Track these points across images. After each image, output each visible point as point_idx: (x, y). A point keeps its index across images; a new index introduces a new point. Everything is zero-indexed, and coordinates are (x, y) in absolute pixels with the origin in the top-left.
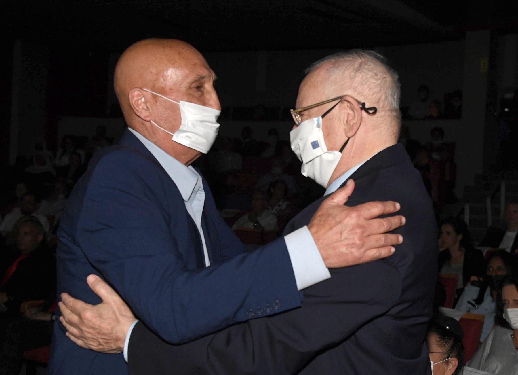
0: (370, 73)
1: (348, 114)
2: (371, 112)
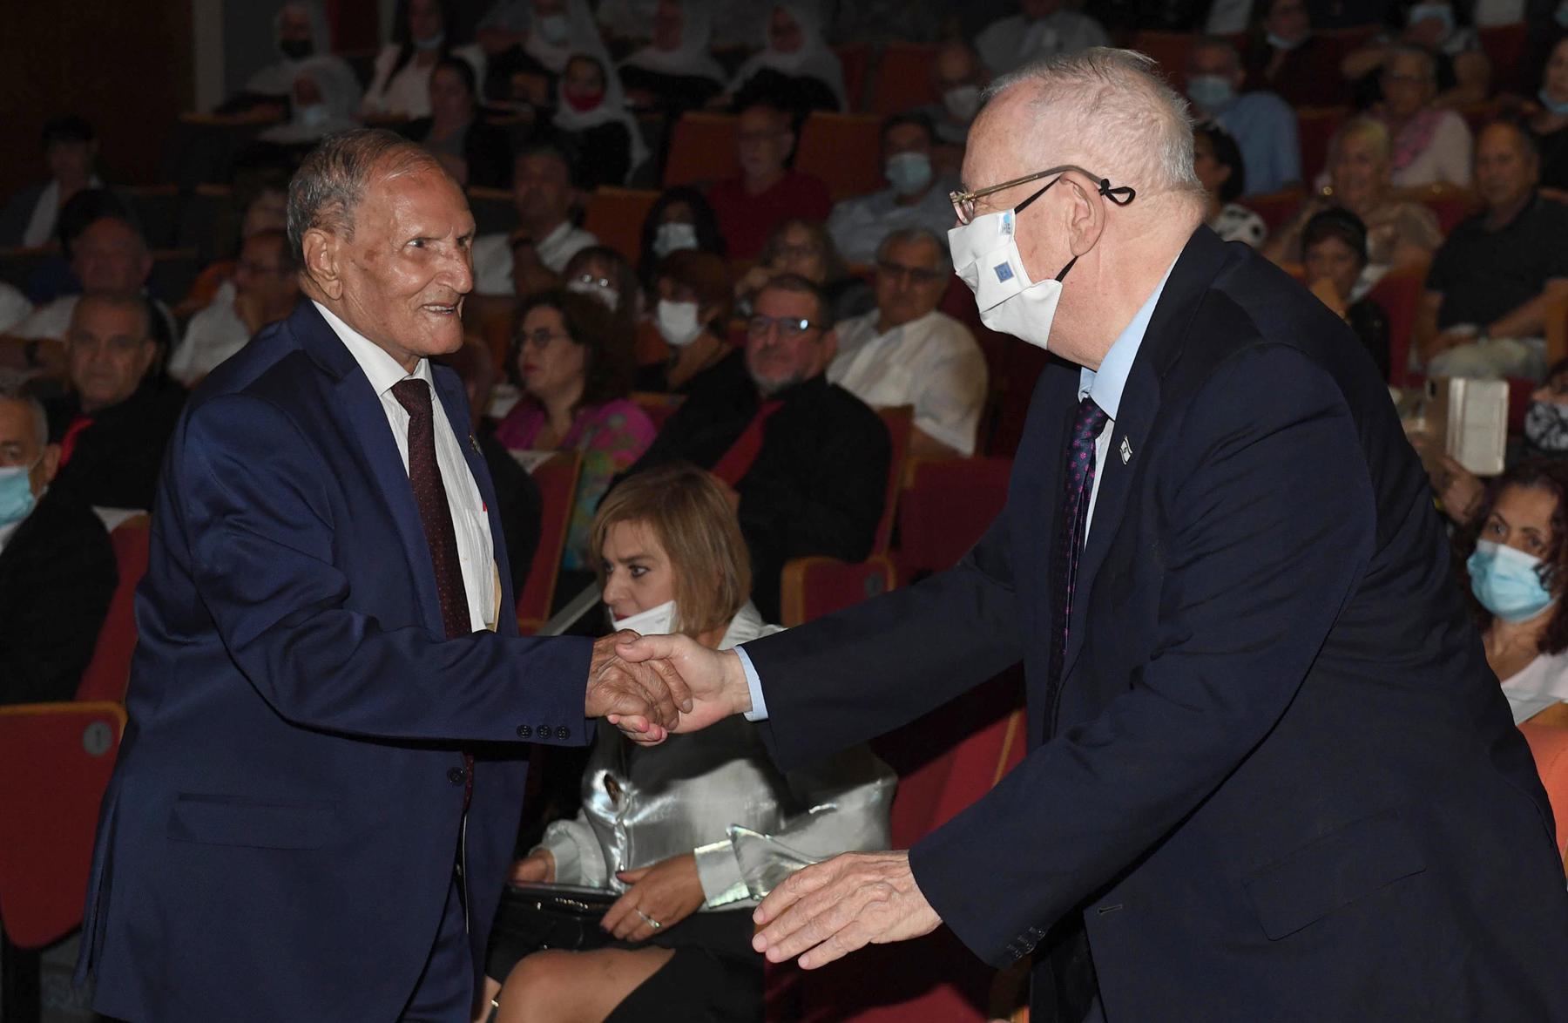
0: (1121, 115)
1: (1077, 206)
2: (1122, 198)
